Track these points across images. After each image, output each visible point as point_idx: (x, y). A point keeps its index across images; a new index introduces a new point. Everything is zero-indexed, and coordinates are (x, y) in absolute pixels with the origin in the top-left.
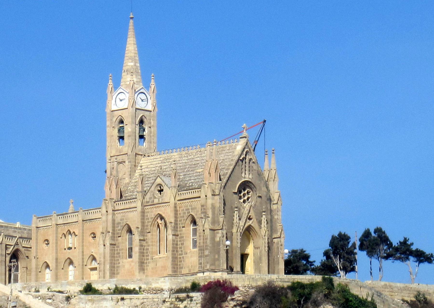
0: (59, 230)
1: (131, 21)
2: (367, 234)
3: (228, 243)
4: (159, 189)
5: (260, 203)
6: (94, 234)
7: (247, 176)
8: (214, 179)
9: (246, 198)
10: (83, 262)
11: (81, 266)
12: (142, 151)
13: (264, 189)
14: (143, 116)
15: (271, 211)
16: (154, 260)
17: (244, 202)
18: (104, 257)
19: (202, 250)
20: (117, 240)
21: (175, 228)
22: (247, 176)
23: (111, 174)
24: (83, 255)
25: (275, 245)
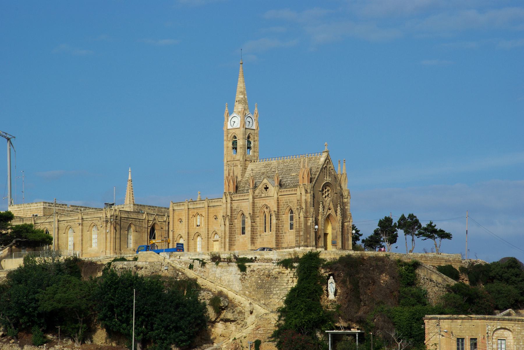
1: (241, 66)
2: (403, 218)
4: (265, 187)
5: (336, 198)
9: (326, 194)
10: (208, 236)
11: (207, 239)
12: (400, 232)
13: (339, 188)
16: (261, 236)
17: (325, 197)
18: (225, 234)
19: (298, 231)
20: (234, 222)
24: (208, 231)
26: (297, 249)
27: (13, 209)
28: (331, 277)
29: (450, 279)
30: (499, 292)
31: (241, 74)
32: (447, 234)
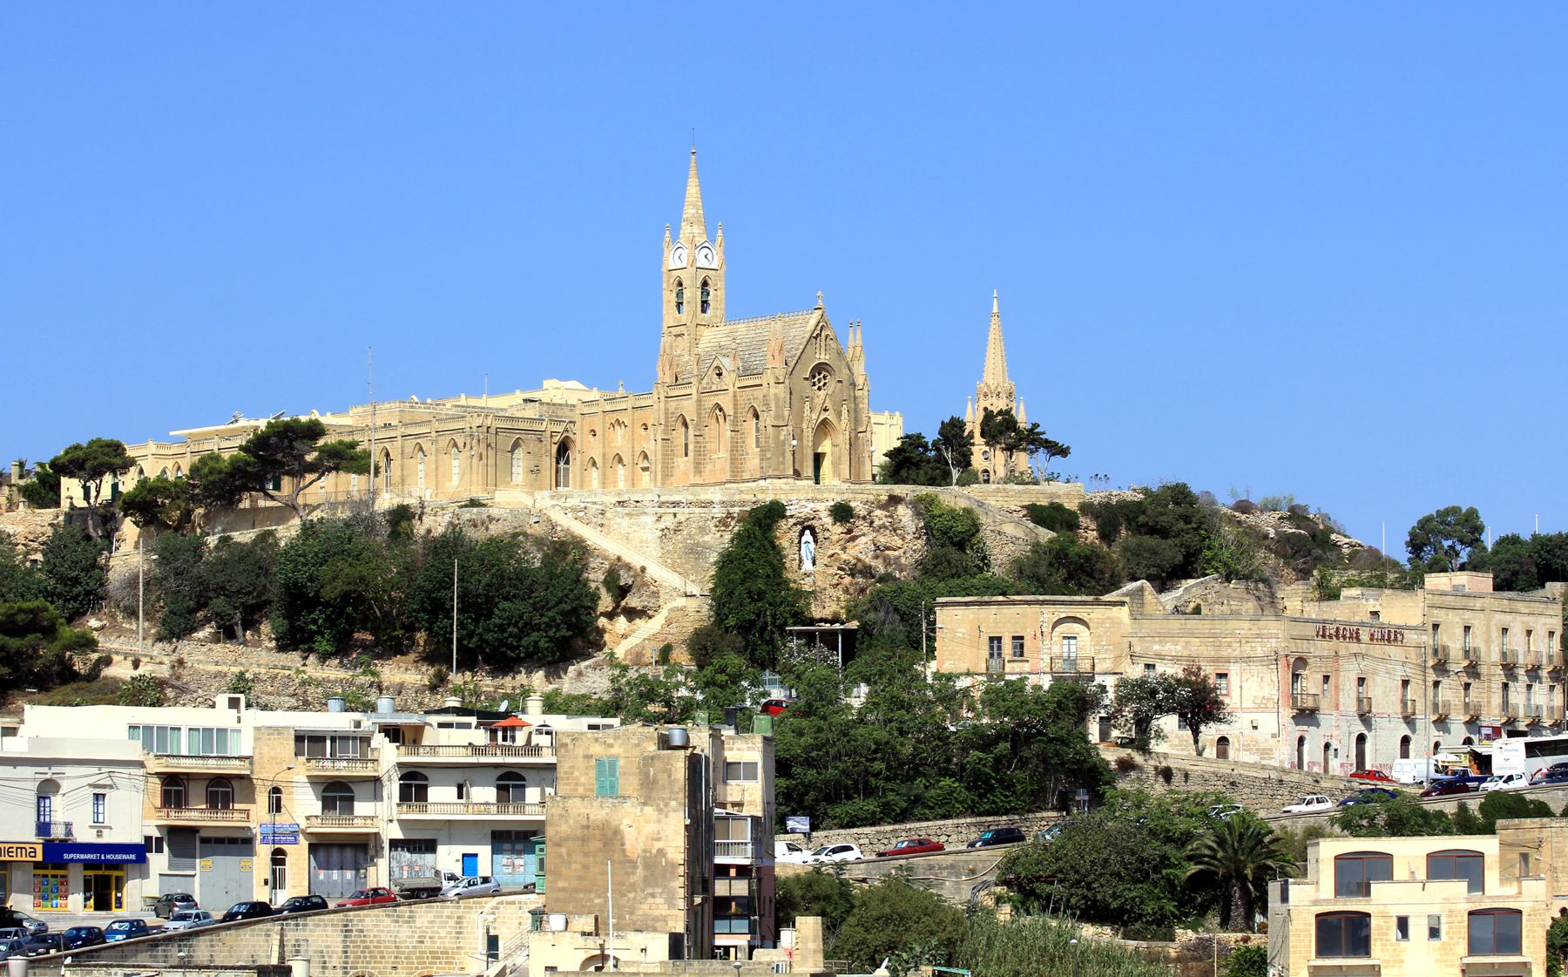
0: (607, 418)
1: (693, 157)
3: (794, 443)
7: (822, 356)
8: (779, 364)
9: (822, 384)
15: (855, 398)
17: (819, 389)
21: (735, 422)
22: (822, 356)
23: (665, 352)
25: (860, 441)
27: (326, 420)
28: (807, 532)
29: (1041, 529)
31: (693, 172)
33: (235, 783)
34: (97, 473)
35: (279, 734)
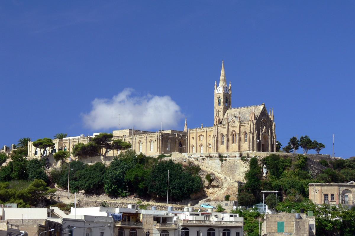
2: (302, 138)
6: (210, 136)
14: (89, 233)
26: (249, 152)
30: (348, 173)
31: (223, 67)
32: (322, 145)
33: (137, 230)
34: (45, 147)
35: (149, 216)
